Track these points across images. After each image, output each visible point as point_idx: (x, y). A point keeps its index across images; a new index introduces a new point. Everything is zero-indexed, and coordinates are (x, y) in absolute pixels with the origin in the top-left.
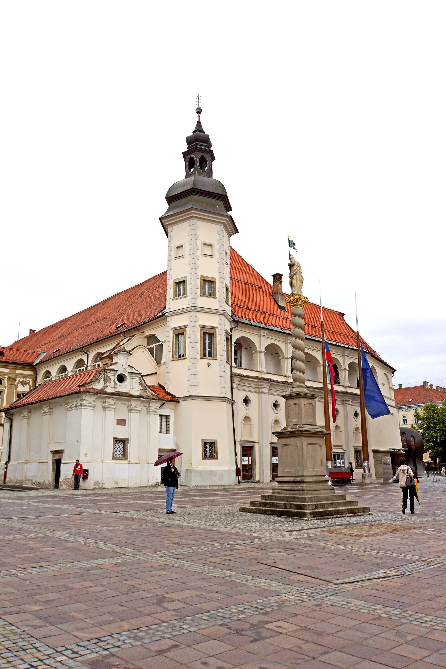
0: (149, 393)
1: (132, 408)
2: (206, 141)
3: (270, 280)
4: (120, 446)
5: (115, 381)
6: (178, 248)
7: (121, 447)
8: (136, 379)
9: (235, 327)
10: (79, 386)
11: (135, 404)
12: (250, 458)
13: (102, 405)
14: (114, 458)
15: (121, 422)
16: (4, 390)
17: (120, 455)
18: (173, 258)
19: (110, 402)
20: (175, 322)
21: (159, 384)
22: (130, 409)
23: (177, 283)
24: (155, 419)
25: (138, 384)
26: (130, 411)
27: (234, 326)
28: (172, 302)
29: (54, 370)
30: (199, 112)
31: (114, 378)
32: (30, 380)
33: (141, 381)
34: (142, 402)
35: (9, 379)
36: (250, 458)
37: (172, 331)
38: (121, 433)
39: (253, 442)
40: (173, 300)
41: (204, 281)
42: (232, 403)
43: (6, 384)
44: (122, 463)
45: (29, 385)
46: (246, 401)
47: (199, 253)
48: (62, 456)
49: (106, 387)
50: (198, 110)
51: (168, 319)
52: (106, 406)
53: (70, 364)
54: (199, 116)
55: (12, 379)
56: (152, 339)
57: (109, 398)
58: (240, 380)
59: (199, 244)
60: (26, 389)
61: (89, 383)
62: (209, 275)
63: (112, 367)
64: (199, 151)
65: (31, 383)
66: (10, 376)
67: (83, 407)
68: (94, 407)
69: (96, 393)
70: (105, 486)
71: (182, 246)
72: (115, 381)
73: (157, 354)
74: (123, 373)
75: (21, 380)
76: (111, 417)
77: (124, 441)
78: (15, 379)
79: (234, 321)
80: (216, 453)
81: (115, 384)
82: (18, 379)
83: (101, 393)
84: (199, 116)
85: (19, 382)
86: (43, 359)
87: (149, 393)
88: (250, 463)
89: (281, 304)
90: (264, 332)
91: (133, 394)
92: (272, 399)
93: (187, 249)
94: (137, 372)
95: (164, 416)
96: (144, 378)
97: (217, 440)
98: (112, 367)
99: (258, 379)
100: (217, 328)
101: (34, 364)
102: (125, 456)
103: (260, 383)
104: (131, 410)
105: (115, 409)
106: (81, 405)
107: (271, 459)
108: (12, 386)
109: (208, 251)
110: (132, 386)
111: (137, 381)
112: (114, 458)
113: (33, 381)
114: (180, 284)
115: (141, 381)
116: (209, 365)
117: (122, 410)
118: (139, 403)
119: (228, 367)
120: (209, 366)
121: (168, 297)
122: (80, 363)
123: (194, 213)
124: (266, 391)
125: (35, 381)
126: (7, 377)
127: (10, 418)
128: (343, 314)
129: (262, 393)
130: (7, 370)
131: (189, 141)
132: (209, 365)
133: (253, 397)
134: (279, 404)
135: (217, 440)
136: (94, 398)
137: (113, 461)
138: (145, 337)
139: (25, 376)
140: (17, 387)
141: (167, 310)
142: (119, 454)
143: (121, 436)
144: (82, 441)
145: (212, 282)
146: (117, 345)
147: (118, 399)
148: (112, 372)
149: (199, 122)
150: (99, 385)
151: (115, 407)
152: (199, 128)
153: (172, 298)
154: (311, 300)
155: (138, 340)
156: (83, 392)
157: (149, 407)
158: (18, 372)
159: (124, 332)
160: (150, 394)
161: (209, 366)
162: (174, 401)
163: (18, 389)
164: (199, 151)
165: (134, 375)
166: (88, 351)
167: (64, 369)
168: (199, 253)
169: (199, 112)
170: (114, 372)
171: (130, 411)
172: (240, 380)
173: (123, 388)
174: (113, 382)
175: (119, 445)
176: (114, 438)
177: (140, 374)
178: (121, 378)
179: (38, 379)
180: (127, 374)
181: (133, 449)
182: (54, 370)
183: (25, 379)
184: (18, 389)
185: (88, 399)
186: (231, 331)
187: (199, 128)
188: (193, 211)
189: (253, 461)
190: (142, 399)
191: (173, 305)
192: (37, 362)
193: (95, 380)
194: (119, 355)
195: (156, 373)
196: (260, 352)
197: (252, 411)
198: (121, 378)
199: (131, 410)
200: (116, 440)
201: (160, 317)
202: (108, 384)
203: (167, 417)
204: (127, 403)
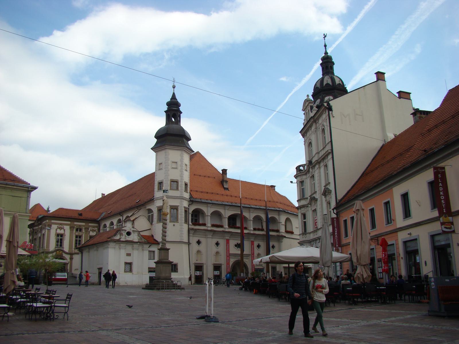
0: (143, 240)
1: (134, 248)
2: (178, 105)
3: (221, 172)
4: (128, 266)
5: (125, 235)
6: (160, 164)
7: (129, 266)
8: (136, 234)
9: (191, 204)
10: (108, 238)
11: (135, 246)
12: (201, 272)
13: (119, 247)
14: (125, 272)
15: (129, 255)
16: (83, 235)
17: (129, 270)
18: (158, 170)
19: (122, 245)
20: (159, 203)
21: (152, 235)
22: (133, 248)
23: (159, 183)
24: (146, 253)
25: (137, 236)
26: (133, 249)
27: (191, 203)
28: (157, 193)
29: (108, 223)
30: (174, 87)
31: (125, 233)
32: (97, 229)
33: (139, 234)
34: (139, 245)
35: (85, 228)
36: (201, 272)
37: (157, 208)
38: (129, 260)
39: (203, 264)
40: (157, 192)
41: (172, 181)
42: (189, 244)
43: (84, 231)
44: (129, 274)
45: (96, 232)
46: (199, 242)
47: (170, 167)
48: (102, 270)
49: (120, 238)
50: (173, 87)
51: (155, 201)
52: (121, 247)
53: (115, 221)
54: (174, 90)
55: (87, 229)
56: (150, 211)
57: (122, 243)
58: (193, 231)
59: (170, 162)
60: (94, 234)
61: (112, 237)
62: (175, 178)
63: (123, 229)
64: (173, 110)
65: (97, 231)
66: (86, 227)
67: (109, 248)
68: (115, 248)
69: (115, 242)
70: (120, 284)
71: (162, 163)
72: (125, 235)
73: (150, 220)
74: (130, 231)
75: (91, 229)
76: (123, 252)
77: (130, 264)
78: (88, 229)
79: (191, 201)
80: (177, 269)
81: (125, 236)
82: (90, 228)
83: (119, 241)
84: (174, 90)
85: (91, 230)
86: (104, 217)
87: (143, 240)
88: (201, 274)
89: (225, 186)
90: (210, 205)
91: (134, 241)
92: (215, 241)
93: (163, 166)
94: (136, 230)
95: (152, 251)
96: (140, 232)
97: (178, 263)
98: (123, 229)
99: (205, 231)
100: (179, 206)
101: (98, 220)
102: (131, 271)
103: (206, 233)
104: (133, 249)
105: (125, 248)
106: (109, 247)
107: (213, 272)
108: (87, 232)
109: (174, 166)
110: (134, 237)
111: (137, 234)
112: (125, 272)
113: (98, 229)
114: (160, 183)
115: (139, 234)
116: (174, 225)
117: (129, 249)
118: (137, 245)
119: (187, 225)
120: (174, 226)
121: (155, 190)
122: (112, 224)
123: (167, 147)
124: (211, 236)
125: (99, 230)
126: (84, 227)
127: (81, 252)
128: (273, 187)
129: (208, 238)
130: (84, 224)
131: (168, 104)
132: (174, 225)
133: (202, 240)
134: (219, 243)
135: (178, 263)
136: (114, 244)
137: (124, 273)
138: (147, 210)
139: (94, 227)
140: (89, 233)
141: (155, 197)
142: (128, 270)
143: (129, 261)
144: (109, 263)
145: (177, 182)
146: (133, 214)
147: (127, 244)
148: (123, 231)
149: (174, 94)
150: (117, 237)
151: (125, 247)
152: (174, 97)
153: (157, 190)
154: (420, 109)
155: (142, 212)
156: (109, 241)
157: (143, 247)
158: (90, 224)
159: (137, 207)
160: (144, 241)
161: (174, 226)
162: (157, 244)
163: (90, 234)
164: (173, 110)
165: (135, 232)
166: (123, 215)
167: (112, 224)
168: (170, 167)
169: (174, 87)
170: (125, 231)
171: (133, 249)
172: (193, 231)
173: (130, 238)
174: (124, 236)
175: (128, 265)
176: (125, 262)
177: (138, 231)
178: (129, 234)
179: (101, 229)
180: (131, 231)
181: (135, 267)
182: (108, 223)
183: (93, 228)
184: (90, 234)
185: (112, 244)
186: (189, 207)
187: (174, 97)
188: (166, 146)
189: (203, 274)
190: (139, 243)
191: (158, 194)
192: (100, 219)
193: (115, 235)
194: (127, 223)
195: (150, 229)
196: (208, 216)
197: (202, 247)
198: (129, 234)
199: (133, 249)
200: (126, 263)
201: (152, 200)
202: (122, 237)
203: (154, 252)
204: (131, 245)
